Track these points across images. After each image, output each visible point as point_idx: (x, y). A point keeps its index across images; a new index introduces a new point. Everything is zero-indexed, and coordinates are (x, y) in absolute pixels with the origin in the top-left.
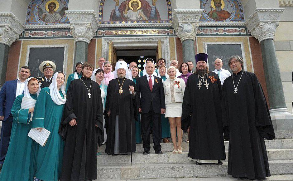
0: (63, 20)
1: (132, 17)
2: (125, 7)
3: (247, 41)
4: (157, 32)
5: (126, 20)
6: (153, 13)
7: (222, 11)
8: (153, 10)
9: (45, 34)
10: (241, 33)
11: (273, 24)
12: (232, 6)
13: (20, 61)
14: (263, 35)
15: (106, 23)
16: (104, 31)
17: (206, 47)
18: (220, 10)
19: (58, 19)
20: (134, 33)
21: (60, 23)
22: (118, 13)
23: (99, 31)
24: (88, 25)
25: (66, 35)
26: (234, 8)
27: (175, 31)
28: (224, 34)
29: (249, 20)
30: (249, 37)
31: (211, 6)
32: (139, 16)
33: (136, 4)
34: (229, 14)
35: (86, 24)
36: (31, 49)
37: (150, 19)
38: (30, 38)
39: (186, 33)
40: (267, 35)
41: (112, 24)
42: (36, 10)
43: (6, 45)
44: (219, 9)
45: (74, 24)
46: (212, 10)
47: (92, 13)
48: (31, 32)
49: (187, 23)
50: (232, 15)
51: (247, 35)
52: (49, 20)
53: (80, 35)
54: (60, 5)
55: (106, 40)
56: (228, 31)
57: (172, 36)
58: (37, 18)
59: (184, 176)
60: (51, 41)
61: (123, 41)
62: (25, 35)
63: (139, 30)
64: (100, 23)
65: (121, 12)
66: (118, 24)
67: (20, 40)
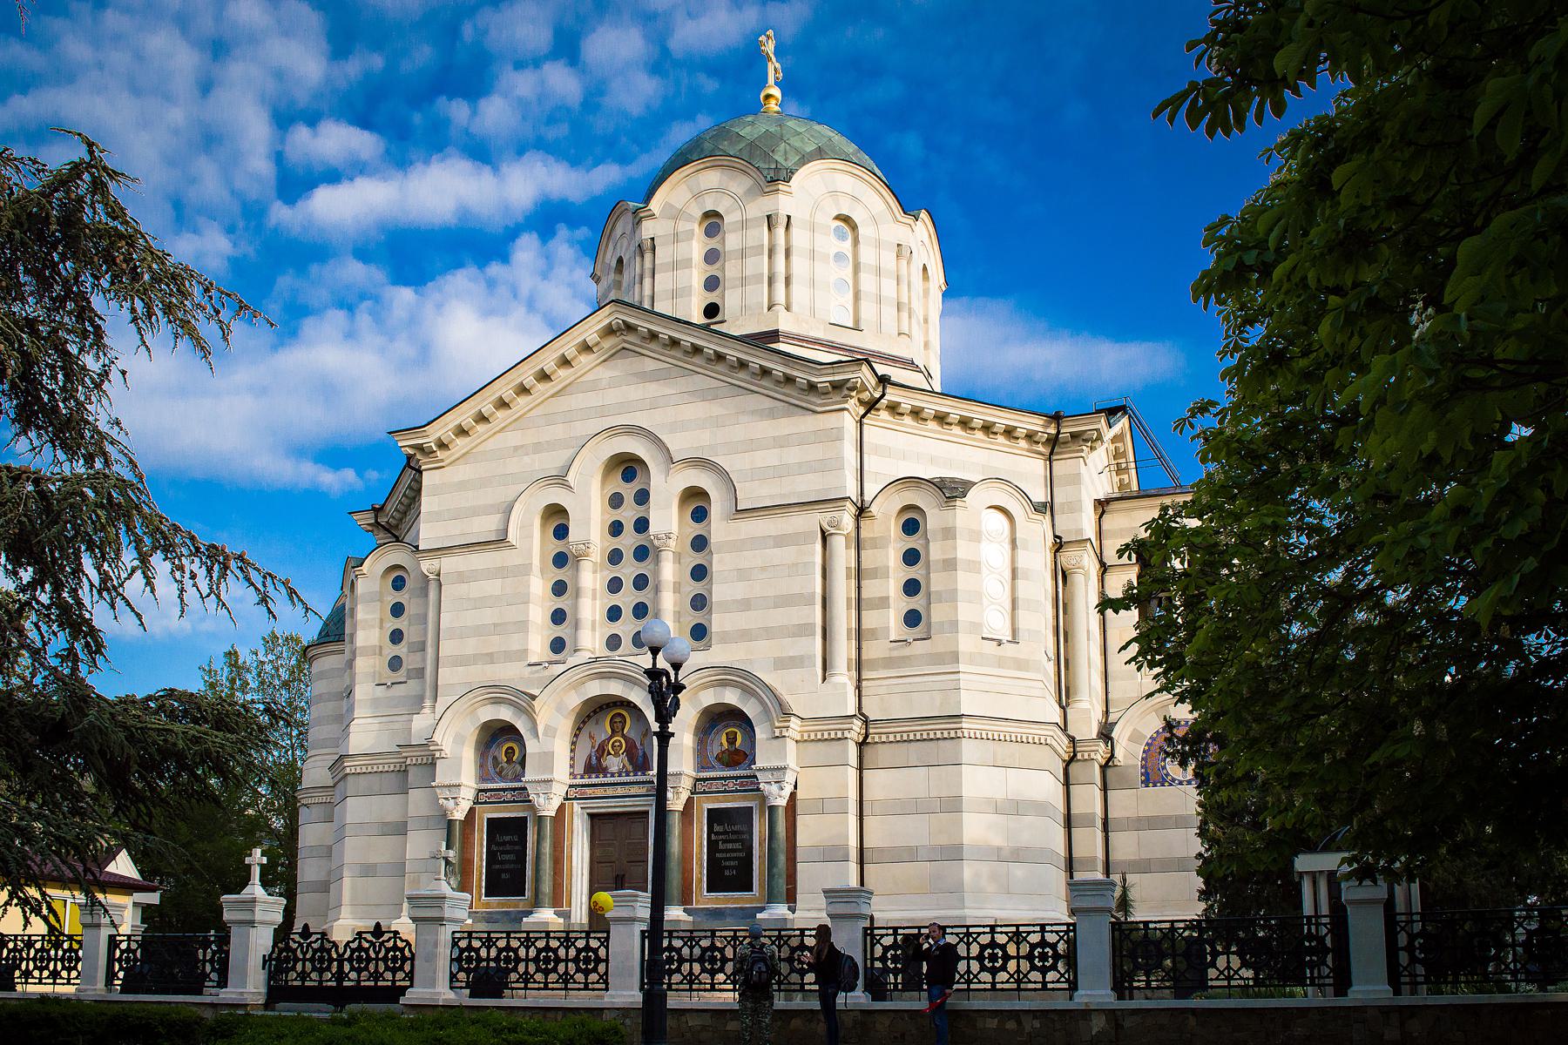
5: (603, 771)
8: (641, 753)
65: (598, 759)
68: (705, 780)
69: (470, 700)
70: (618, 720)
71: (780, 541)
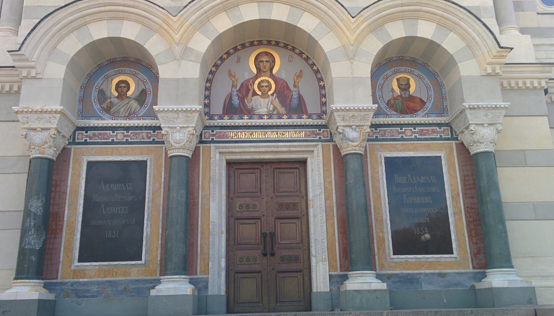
0: (142, 112)
1: (259, 107)
2: (248, 90)
3: (453, 152)
4: (302, 135)
5: (251, 113)
6: (295, 102)
8: (295, 95)
9: (112, 136)
10: (443, 137)
11: (492, 128)
13: (69, 184)
14: (475, 145)
15: (216, 118)
16: (213, 131)
17: (383, 161)
18: (407, 96)
19: (134, 109)
20: (264, 137)
21: (138, 118)
22: (236, 101)
23: (205, 133)
24: (190, 129)
25: (149, 138)
26: (432, 93)
27: (331, 133)
28: (413, 137)
29: (454, 116)
30: (456, 144)
31: (392, 89)
32: (272, 106)
33: (266, 84)
36: (90, 164)
38: (86, 143)
39: (350, 143)
40: (482, 145)
41: (227, 121)
43: (50, 161)
44: (405, 94)
45: (169, 127)
46: (393, 96)
47: (198, 111)
48: (87, 132)
49: (350, 126)
50: (427, 104)
51: (452, 139)
52: (118, 112)
53: (177, 146)
54: (137, 85)
55: (217, 148)
56: (421, 131)
58: (97, 107)
61: (246, 150)
62: (76, 139)
63: (272, 132)
64: (207, 117)
65: (242, 99)
67: (69, 146)
68: (87, 129)
70: (265, 58)
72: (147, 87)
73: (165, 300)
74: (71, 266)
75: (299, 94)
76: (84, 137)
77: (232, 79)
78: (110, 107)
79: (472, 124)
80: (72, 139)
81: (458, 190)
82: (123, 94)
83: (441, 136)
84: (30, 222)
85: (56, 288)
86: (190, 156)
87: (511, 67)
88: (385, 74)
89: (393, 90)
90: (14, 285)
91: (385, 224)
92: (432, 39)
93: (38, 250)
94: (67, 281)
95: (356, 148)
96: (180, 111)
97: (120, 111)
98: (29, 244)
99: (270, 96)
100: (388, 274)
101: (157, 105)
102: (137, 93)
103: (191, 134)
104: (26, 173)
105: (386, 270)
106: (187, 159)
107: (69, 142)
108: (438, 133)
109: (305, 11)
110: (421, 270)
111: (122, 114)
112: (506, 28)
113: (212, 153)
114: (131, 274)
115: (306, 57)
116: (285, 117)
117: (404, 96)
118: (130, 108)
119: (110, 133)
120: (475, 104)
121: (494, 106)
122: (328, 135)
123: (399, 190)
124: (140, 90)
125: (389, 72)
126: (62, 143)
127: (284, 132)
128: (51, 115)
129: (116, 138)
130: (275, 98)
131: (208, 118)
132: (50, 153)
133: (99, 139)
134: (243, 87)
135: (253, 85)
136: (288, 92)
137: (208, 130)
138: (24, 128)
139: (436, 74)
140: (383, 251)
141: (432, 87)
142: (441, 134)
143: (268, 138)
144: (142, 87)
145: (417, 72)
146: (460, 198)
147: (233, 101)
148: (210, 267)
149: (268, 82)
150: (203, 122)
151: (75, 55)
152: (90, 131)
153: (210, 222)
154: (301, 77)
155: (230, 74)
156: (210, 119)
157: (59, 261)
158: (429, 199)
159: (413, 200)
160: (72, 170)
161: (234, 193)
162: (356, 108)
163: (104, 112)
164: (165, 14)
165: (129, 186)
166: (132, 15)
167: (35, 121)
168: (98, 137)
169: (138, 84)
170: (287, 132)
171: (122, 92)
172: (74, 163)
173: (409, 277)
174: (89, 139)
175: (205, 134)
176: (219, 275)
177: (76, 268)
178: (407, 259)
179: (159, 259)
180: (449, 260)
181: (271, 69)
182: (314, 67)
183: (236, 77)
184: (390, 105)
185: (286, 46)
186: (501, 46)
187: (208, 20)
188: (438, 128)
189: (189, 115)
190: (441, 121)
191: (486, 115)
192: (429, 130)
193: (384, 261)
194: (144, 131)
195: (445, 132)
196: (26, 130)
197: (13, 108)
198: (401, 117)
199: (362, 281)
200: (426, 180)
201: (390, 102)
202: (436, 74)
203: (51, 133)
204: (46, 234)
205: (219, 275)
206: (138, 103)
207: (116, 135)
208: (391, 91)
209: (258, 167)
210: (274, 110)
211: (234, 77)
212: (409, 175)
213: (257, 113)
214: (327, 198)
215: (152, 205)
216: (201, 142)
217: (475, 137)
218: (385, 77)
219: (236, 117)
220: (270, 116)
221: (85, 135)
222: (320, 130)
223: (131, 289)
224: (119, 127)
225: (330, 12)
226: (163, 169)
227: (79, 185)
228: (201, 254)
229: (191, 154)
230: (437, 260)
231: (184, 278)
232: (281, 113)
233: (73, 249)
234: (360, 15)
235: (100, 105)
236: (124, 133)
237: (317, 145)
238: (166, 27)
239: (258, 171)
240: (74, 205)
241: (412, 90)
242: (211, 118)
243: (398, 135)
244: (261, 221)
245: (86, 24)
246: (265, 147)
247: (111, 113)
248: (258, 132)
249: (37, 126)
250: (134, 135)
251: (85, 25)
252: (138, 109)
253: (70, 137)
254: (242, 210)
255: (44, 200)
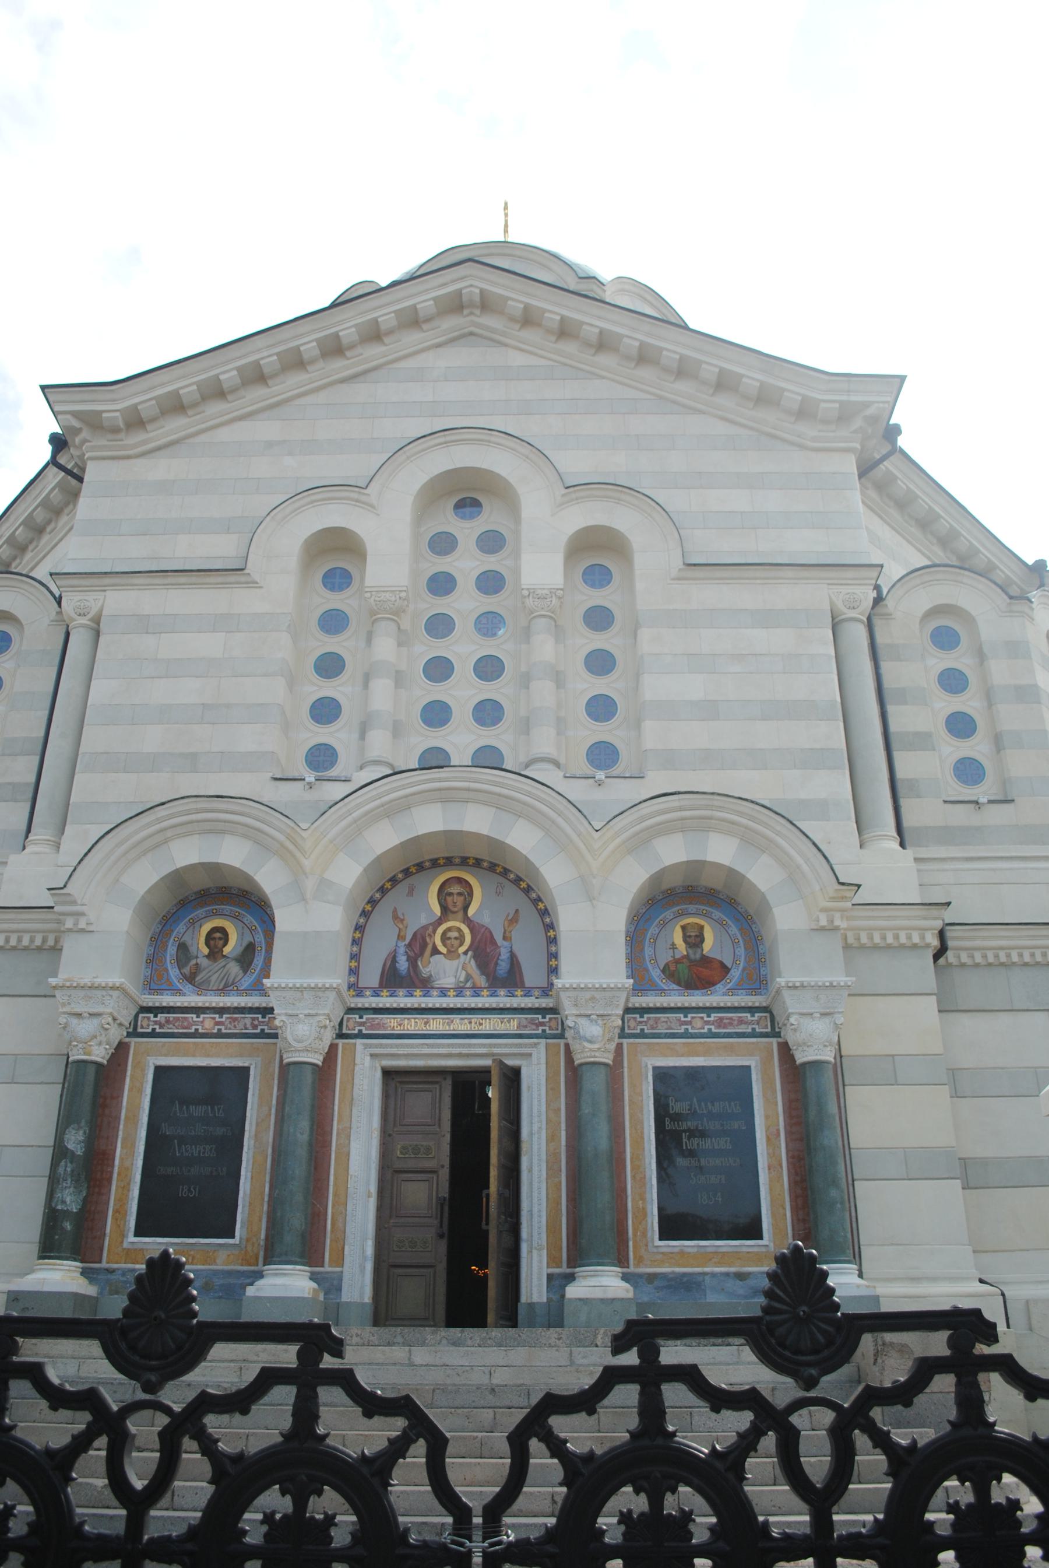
0: (247, 982)
2: (424, 945)
3: (772, 1057)
4: (512, 1024)
5: (425, 984)
6: (503, 966)
7: (706, 961)
8: (504, 955)
9: (195, 1023)
10: (757, 1030)
11: (827, 1020)
12: (734, 943)
13: (124, 1103)
14: (800, 1048)
15: (368, 993)
18: (698, 956)
20: (447, 1028)
21: (240, 993)
22: (403, 964)
23: (348, 1020)
24: (321, 1018)
25: (255, 1027)
26: (741, 951)
31: (673, 944)
32: (464, 973)
33: (455, 934)
34: (725, 970)
35: (317, 1015)
36: (159, 1070)
37: (495, 983)
38: (153, 1034)
39: (586, 1044)
41: (385, 1001)
42: (172, 950)
43: (98, 1065)
44: (695, 954)
45: (286, 1014)
46: (674, 957)
48: (156, 1016)
50: (732, 971)
52: (208, 981)
53: (299, 1046)
54: (241, 936)
55: (366, 1046)
56: (720, 1023)
57: (554, 1037)
58: (174, 973)
59: (511, 1404)
60: (212, 1047)
61: (415, 1051)
62: (139, 1027)
64: (352, 992)
65: (413, 961)
66: (402, 1000)
68: (643, 1011)
69: (159, 820)
70: (456, 889)
71: (766, 618)
72: (256, 939)
73: (268, 1304)
74: (122, 1242)
75: (511, 951)
76: (151, 1023)
77: (398, 925)
78: (195, 973)
79: (792, 1013)
80: (132, 1027)
81: (778, 1125)
82: (217, 950)
83: (754, 1029)
84: (66, 1167)
85: (99, 1277)
86: (320, 1063)
87: (872, 910)
88: (661, 918)
89: (673, 947)
90: (39, 1267)
91: (648, 1186)
92: (731, 866)
93: (76, 1212)
94: (115, 1266)
95: (597, 1054)
96: (305, 988)
97: (210, 981)
98: (64, 1202)
99: (461, 955)
100: (649, 1274)
101: (268, 977)
102: (240, 949)
103: (321, 1027)
104: (59, 1083)
105: (646, 1266)
106: (315, 1067)
107: (128, 1033)
108: (750, 1024)
109: (520, 816)
110: (707, 1267)
111: (213, 986)
112: (874, 836)
113: (358, 1056)
114: (218, 1261)
115: (526, 886)
116: (485, 992)
117: (692, 956)
118: (226, 977)
119: (192, 1018)
120: (797, 979)
121: (827, 984)
122: (558, 1025)
123: (676, 1125)
124: (245, 944)
125: (669, 914)
126: (116, 1034)
127: (482, 1019)
128: (104, 993)
129: (203, 1026)
130: (470, 959)
131: (354, 993)
132: (100, 1054)
133: (174, 1027)
134: (416, 941)
135: (433, 935)
136: (492, 948)
137: (354, 1014)
138: (64, 1013)
139: (750, 917)
140: (643, 1233)
141: (741, 941)
142: (754, 1026)
143: (454, 1030)
144: (248, 938)
145: (717, 914)
146: (780, 1141)
147: (397, 965)
148: (345, 1253)
149: (459, 930)
150: (343, 1002)
151: (146, 893)
152: (161, 1013)
153: (349, 1177)
154: (517, 922)
155: (396, 917)
156: (357, 995)
157: (105, 1234)
158: (726, 1142)
159: (698, 1144)
160: (131, 1080)
161: (395, 1125)
162: (597, 986)
163: (185, 981)
164: (290, 826)
165: (219, 1110)
166: (238, 826)
167: (80, 1002)
168: (174, 1025)
169: (243, 933)
170: (488, 1020)
171: (216, 946)
172: (134, 1067)
173: (685, 1279)
174: (160, 1028)
175: (348, 1021)
176: (363, 1269)
177: (130, 1246)
178: (683, 1248)
179: (263, 1236)
180: (755, 1249)
181: (466, 908)
182: (540, 903)
183: (405, 922)
184: (667, 972)
185: (492, 867)
186: (841, 881)
187: (359, 832)
188: (748, 1015)
189: (320, 994)
190: (754, 1003)
191: (817, 998)
192: (734, 1018)
193: (643, 1250)
194: (247, 1016)
195: (757, 1022)
196: (66, 1016)
197: (50, 980)
198: (686, 994)
199: (593, 1284)
200: (723, 1107)
201: (669, 968)
202: (750, 917)
203: (103, 1022)
204: (88, 1188)
205: (363, 1269)
206: (241, 967)
207: (202, 1022)
208: (670, 948)
209: (437, 1080)
210: (467, 981)
211: (402, 921)
212: (695, 1100)
213: (437, 986)
214: (552, 1138)
215: (255, 1143)
216: (341, 1036)
217: (798, 1036)
218: (662, 922)
219: (401, 992)
220: (459, 992)
221: (154, 1021)
222: (544, 1017)
223: (217, 1285)
224: (208, 1008)
225: (560, 820)
226: (276, 1082)
227: (139, 1107)
228: (332, 1232)
229: (321, 1058)
230: (735, 1250)
231: (300, 1270)
232: (479, 986)
233: (126, 1214)
234: (608, 826)
235: (180, 969)
236: (214, 1018)
237: (538, 1043)
238: (291, 847)
239: (437, 1086)
240: (130, 1144)
241: (708, 944)
242: (360, 993)
243: (679, 1028)
244: (438, 1177)
245: (166, 841)
246: (449, 1046)
247: (196, 983)
248: (438, 1020)
249: (83, 1010)
250: (230, 1023)
251: (165, 843)
252: (240, 977)
253: (130, 1024)
254: (407, 1156)
255: (87, 1131)
